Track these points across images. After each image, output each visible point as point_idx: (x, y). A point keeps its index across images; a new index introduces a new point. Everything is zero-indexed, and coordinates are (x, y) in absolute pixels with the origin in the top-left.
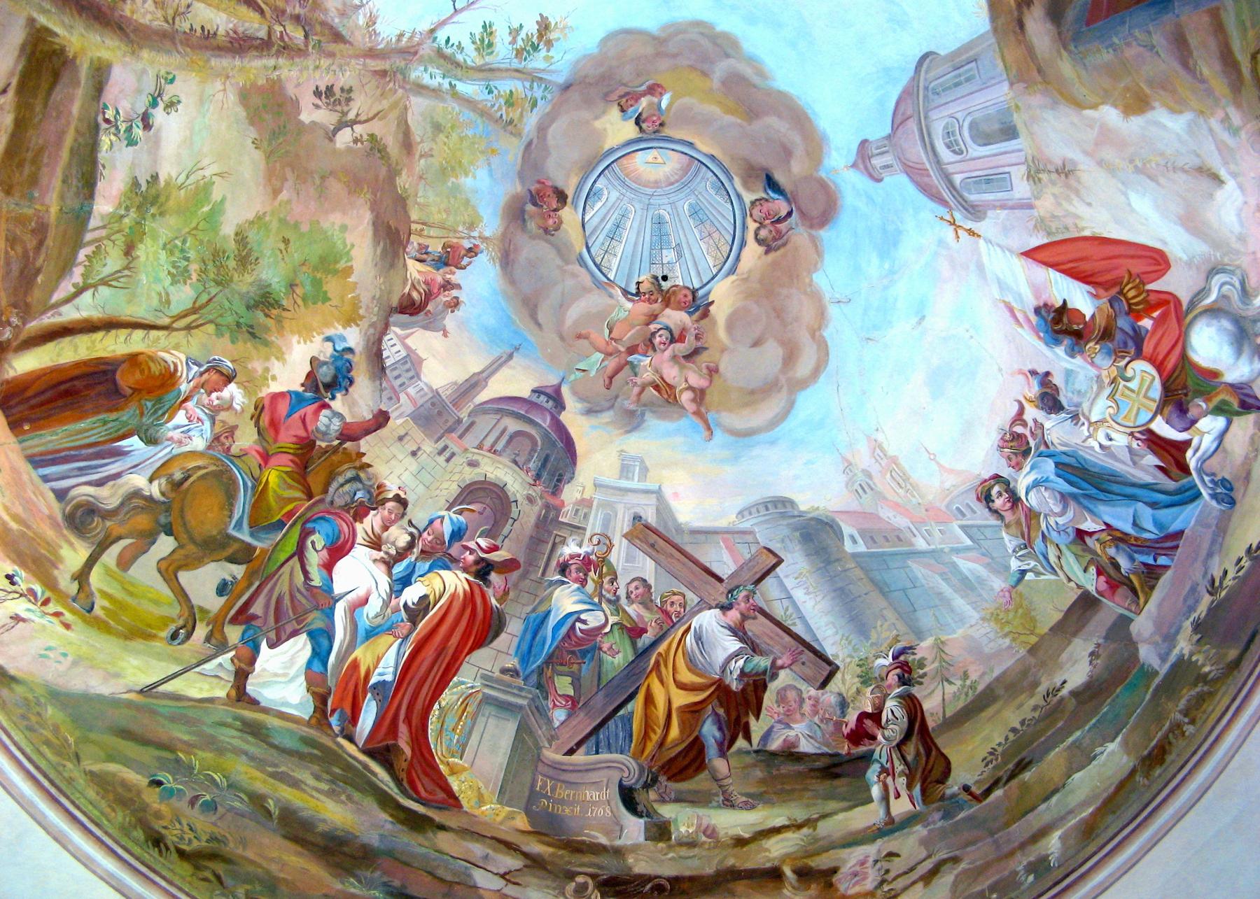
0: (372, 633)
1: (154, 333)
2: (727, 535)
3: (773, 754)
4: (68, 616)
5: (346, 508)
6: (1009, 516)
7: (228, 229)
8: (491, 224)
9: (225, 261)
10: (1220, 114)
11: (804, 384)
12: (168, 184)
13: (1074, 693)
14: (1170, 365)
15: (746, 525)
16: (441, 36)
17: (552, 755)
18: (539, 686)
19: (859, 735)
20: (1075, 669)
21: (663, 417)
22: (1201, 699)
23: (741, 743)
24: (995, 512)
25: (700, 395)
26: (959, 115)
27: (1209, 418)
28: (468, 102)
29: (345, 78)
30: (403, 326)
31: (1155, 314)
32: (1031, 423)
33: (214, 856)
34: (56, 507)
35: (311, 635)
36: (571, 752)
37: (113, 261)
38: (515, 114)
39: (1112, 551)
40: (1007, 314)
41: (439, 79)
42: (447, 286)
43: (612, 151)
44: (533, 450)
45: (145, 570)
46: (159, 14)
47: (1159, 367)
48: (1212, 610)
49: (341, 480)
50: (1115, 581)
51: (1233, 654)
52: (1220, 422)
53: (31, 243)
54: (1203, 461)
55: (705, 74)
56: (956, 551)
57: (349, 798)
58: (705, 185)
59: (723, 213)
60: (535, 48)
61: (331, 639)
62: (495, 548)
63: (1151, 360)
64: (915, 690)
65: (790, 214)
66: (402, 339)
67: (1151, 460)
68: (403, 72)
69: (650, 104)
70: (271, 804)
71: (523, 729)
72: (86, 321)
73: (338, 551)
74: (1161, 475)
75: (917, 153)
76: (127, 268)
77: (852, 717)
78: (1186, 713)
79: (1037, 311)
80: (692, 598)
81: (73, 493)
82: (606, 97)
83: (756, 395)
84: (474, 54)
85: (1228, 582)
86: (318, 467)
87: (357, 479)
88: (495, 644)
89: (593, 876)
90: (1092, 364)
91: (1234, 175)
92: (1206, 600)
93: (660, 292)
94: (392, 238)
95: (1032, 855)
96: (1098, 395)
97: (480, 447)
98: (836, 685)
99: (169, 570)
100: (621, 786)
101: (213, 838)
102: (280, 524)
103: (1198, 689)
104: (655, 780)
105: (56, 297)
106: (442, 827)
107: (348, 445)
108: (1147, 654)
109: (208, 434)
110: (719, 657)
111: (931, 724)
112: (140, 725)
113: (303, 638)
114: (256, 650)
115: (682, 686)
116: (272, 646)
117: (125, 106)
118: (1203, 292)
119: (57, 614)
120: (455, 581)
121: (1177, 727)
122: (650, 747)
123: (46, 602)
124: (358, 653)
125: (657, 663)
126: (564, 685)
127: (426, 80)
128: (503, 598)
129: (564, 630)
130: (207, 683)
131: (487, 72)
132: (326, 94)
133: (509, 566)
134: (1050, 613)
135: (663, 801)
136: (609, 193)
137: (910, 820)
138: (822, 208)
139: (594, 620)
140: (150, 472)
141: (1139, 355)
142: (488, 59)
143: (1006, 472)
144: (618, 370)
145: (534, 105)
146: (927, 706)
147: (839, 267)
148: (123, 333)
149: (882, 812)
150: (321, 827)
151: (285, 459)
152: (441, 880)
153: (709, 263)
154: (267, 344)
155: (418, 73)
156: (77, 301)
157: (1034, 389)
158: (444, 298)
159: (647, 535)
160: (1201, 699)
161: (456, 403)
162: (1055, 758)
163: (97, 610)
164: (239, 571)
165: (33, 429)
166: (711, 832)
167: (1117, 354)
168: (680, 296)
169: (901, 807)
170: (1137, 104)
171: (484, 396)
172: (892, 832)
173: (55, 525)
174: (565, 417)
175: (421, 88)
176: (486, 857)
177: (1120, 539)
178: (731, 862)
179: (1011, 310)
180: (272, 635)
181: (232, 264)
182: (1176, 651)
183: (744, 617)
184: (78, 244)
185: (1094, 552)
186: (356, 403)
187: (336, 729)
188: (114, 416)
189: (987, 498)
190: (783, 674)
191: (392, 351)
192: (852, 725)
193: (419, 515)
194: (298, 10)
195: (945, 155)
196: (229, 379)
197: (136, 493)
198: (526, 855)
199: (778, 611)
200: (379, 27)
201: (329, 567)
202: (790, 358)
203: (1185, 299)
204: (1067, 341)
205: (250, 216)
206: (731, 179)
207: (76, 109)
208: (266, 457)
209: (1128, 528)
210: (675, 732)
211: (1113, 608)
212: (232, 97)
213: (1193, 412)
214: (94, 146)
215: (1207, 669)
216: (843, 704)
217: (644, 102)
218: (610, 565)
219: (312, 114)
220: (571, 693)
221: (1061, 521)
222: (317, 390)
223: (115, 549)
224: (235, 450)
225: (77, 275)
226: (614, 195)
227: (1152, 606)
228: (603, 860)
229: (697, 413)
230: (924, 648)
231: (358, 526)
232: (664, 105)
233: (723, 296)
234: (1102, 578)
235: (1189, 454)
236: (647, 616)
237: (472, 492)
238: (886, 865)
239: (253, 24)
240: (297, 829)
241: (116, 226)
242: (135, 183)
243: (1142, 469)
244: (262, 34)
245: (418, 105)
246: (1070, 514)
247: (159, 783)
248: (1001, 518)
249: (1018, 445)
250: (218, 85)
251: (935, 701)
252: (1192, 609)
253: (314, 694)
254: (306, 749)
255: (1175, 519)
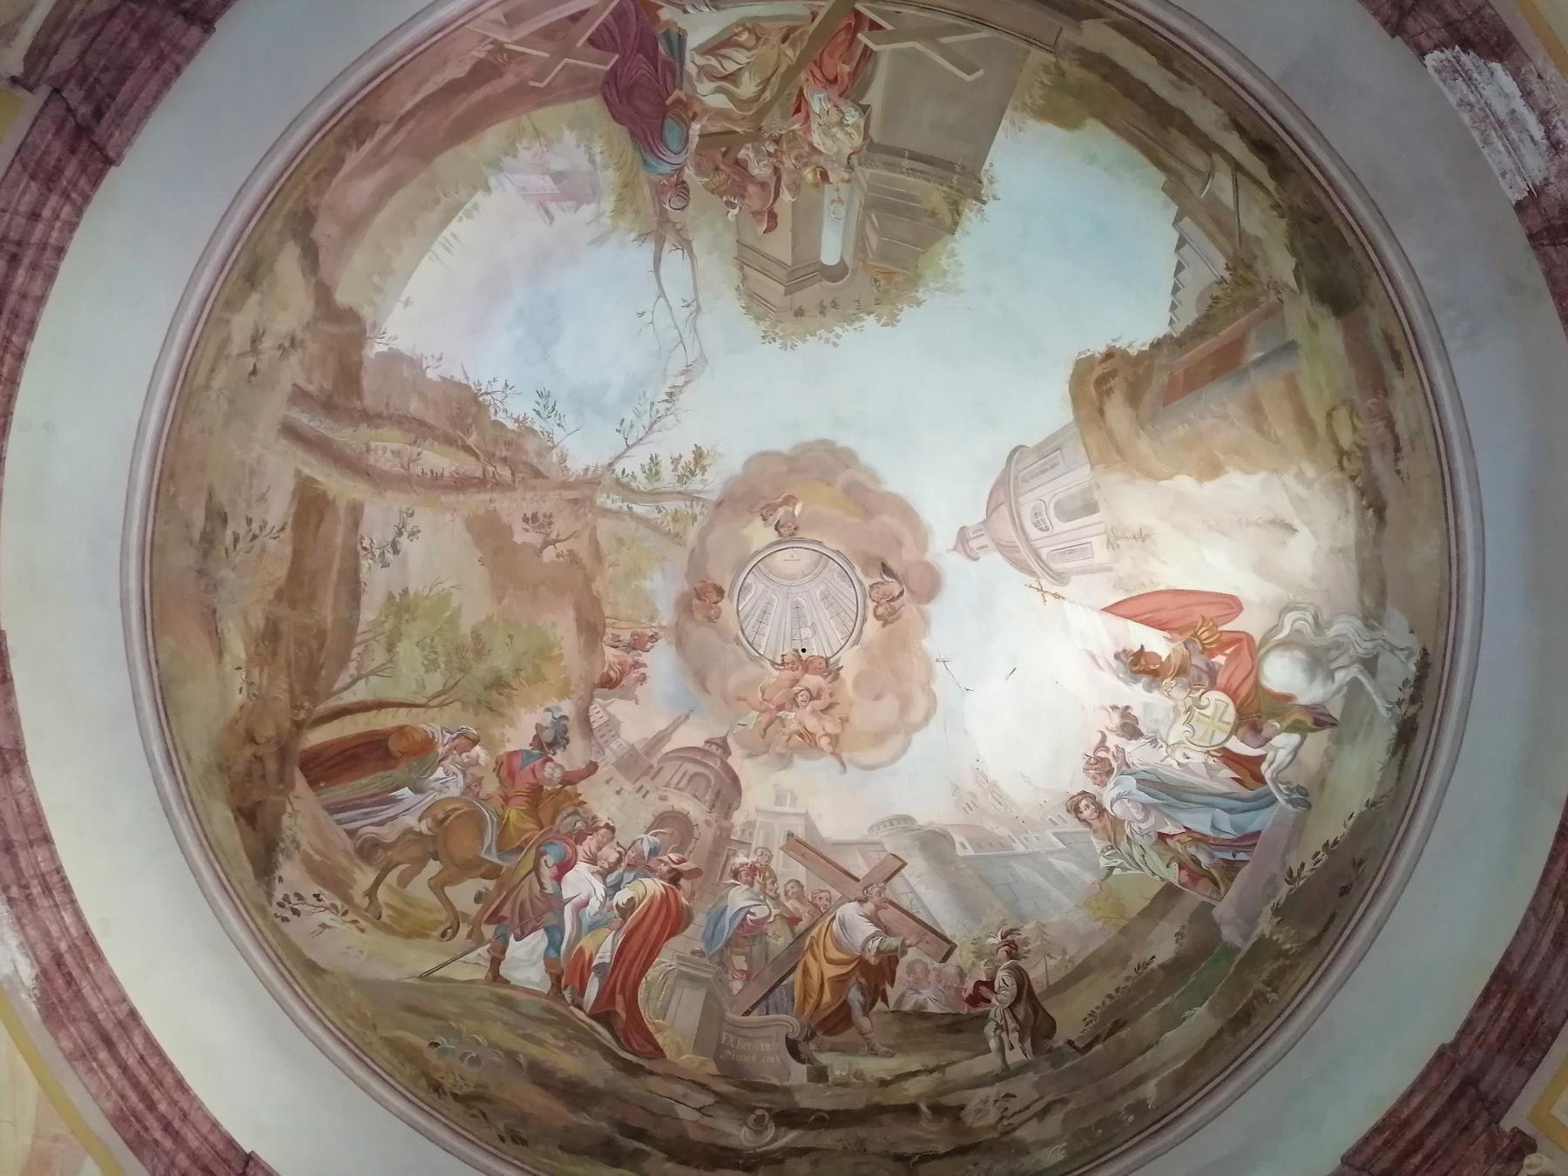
0: (594, 927)
1: (415, 710)
2: (862, 845)
3: (906, 1014)
4: (363, 923)
5: (569, 834)
6: (1096, 824)
7: (466, 627)
8: (666, 615)
9: (463, 654)
10: (1294, 469)
11: (917, 727)
12: (416, 595)
13: (1162, 967)
14: (1244, 692)
15: (875, 837)
16: (618, 468)
17: (733, 1015)
18: (721, 963)
19: (976, 999)
20: (1163, 946)
21: (807, 757)
22: (1281, 973)
23: (880, 1005)
24: (1084, 821)
25: (835, 740)
26: (1046, 498)
27: (1283, 735)
28: (639, 519)
29: (545, 508)
30: (605, 697)
31: (1228, 651)
32: (1113, 749)
33: (479, 1098)
34: (348, 843)
35: (547, 930)
36: (747, 1013)
37: (379, 657)
38: (679, 528)
39: (1192, 850)
40: (1090, 660)
41: (619, 504)
42: (636, 665)
43: (757, 553)
44: (708, 786)
45: (419, 888)
46: (397, 461)
47: (1233, 696)
48: (1290, 898)
49: (564, 814)
50: (1196, 873)
51: (1312, 933)
52: (1295, 738)
53: (314, 645)
54: (1279, 771)
55: (829, 484)
56: (1052, 853)
57: (580, 1052)
58: (832, 573)
59: (848, 596)
60: (693, 474)
61: (562, 932)
62: (683, 861)
63: (1225, 690)
64: (1022, 963)
65: (901, 593)
66: (604, 708)
67: (1227, 773)
68: (591, 500)
69: (786, 513)
70: (522, 1059)
71: (710, 996)
72: (362, 702)
73: (564, 867)
74: (1237, 785)
75: (1008, 533)
76: (391, 661)
77: (969, 985)
78: (1268, 983)
79: (1117, 656)
80: (836, 894)
81: (361, 831)
82: (750, 510)
83: (880, 737)
84: (645, 481)
85: (1306, 872)
86: (545, 804)
87: (576, 813)
88: (686, 932)
89: (769, 1110)
90: (1169, 696)
91: (1308, 524)
92: (1285, 889)
93: (801, 662)
94: (591, 630)
95: (1131, 1098)
96: (1174, 722)
97: (667, 785)
98: (955, 959)
99: (438, 886)
100: (787, 1039)
101: (477, 1086)
102: (520, 849)
103: (1279, 963)
104: (813, 1034)
105: (337, 686)
106: (651, 1073)
107: (568, 788)
108: (1229, 934)
109: (461, 784)
110: (860, 939)
111: (1037, 991)
112: (419, 1001)
113: (542, 931)
114: (506, 943)
115: (830, 961)
116: (517, 939)
117: (377, 537)
118: (1277, 627)
119: (355, 922)
120: (654, 886)
121: (1259, 996)
122: (808, 1009)
123: (345, 913)
124: (583, 943)
125: (811, 945)
126: (740, 962)
127: (609, 504)
128: (691, 897)
129: (738, 920)
130: (470, 969)
131: (655, 495)
132: (532, 519)
133: (694, 873)
134: (1137, 902)
135: (820, 1050)
136: (756, 585)
137: (1023, 1068)
138: (930, 585)
139: (761, 912)
140: (418, 814)
141: (1213, 686)
142: (656, 485)
143: (1092, 789)
144: (769, 724)
145: (695, 519)
146: (1032, 975)
147: (945, 631)
148: (391, 710)
149: (999, 1062)
150: (559, 1075)
151: (522, 800)
152: (653, 1114)
153: (837, 637)
154: (502, 715)
155: (605, 500)
156: (354, 688)
157: (1116, 720)
158: (634, 674)
159: (799, 847)
160: (1281, 973)
161: (647, 754)
162: (1149, 1018)
163: (384, 918)
164: (490, 884)
165: (327, 786)
166: (859, 1075)
167: (1192, 686)
168: (816, 664)
169: (1015, 1056)
170: (1212, 470)
171: (668, 747)
172: (1008, 1077)
173: (349, 856)
174: (731, 761)
175: (606, 512)
176: (685, 1096)
177: (1200, 839)
178: (877, 1099)
179: (1093, 657)
180: (518, 931)
181: (470, 655)
182: (1258, 931)
183: (878, 908)
184: (350, 645)
185: (1175, 851)
186: (571, 757)
187: (569, 1000)
188: (389, 772)
189: (1075, 810)
190: (911, 951)
191: (597, 718)
192: (970, 991)
193: (624, 838)
194: (504, 453)
195: (1034, 533)
196: (475, 742)
197: (409, 830)
198: (715, 1093)
199: (905, 902)
200: (569, 464)
201: (558, 878)
202: (905, 705)
203: (1258, 637)
204: (1145, 679)
205: (483, 618)
206: (853, 568)
207: (339, 540)
208: (506, 800)
209: (1207, 831)
210: (827, 997)
211: (1196, 896)
212: (459, 526)
213: (1266, 732)
214: (356, 570)
215: (1287, 946)
216: (962, 974)
217: (781, 511)
218: (771, 871)
219: (523, 536)
220: (745, 968)
221: (1144, 826)
222: (542, 748)
223: (395, 873)
224: (482, 795)
225: (352, 668)
226: (761, 587)
227: (1232, 893)
228: (777, 1097)
229: (833, 753)
230: (1028, 930)
231: (579, 847)
232: (797, 513)
233: (850, 663)
234: (1184, 873)
235: (1264, 766)
236: (801, 908)
237: (661, 820)
238: (1005, 1104)
239: (471, 467)
240: (541, 1076)
241: (379, 630)
242: (391, 596)
243: (1218, 780)
244: (479, 474)
245: (605, 526)
246: (1152, 821)
247: (437, 1045)
248: (1090, 825)
249: (1101, 767)
250: (448, 517)
251: (1038, 972)
252: (1270, 897)
253: (551, 974)
254: (546, 1016)
255: (1253, 820)
